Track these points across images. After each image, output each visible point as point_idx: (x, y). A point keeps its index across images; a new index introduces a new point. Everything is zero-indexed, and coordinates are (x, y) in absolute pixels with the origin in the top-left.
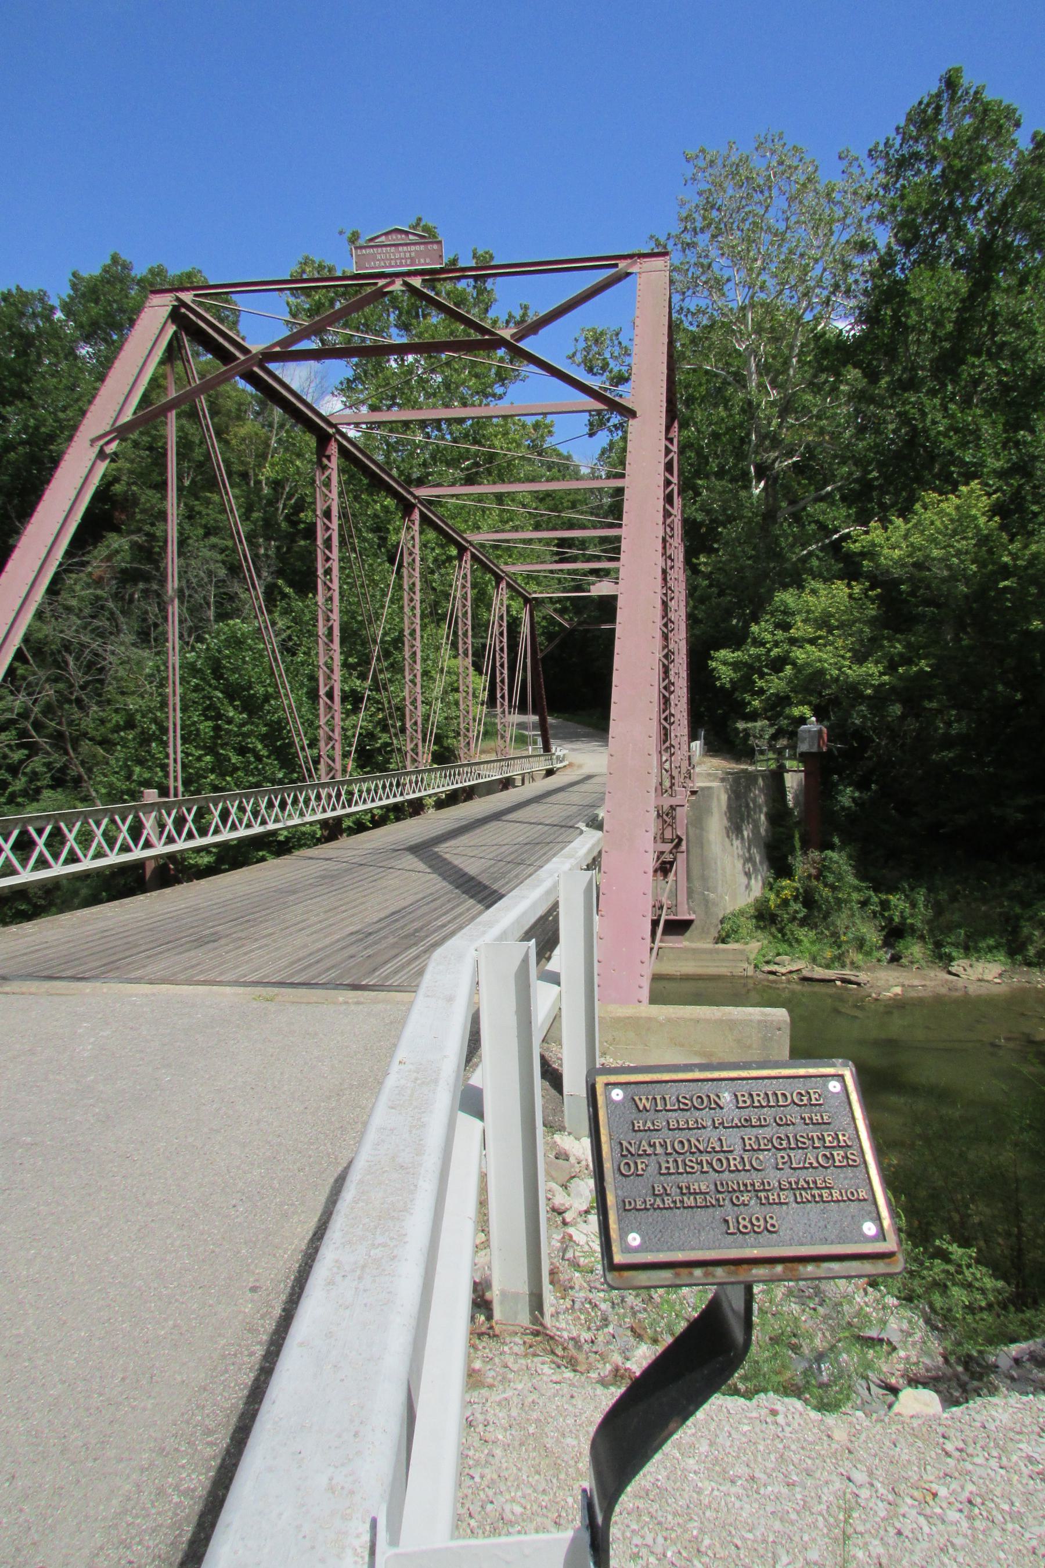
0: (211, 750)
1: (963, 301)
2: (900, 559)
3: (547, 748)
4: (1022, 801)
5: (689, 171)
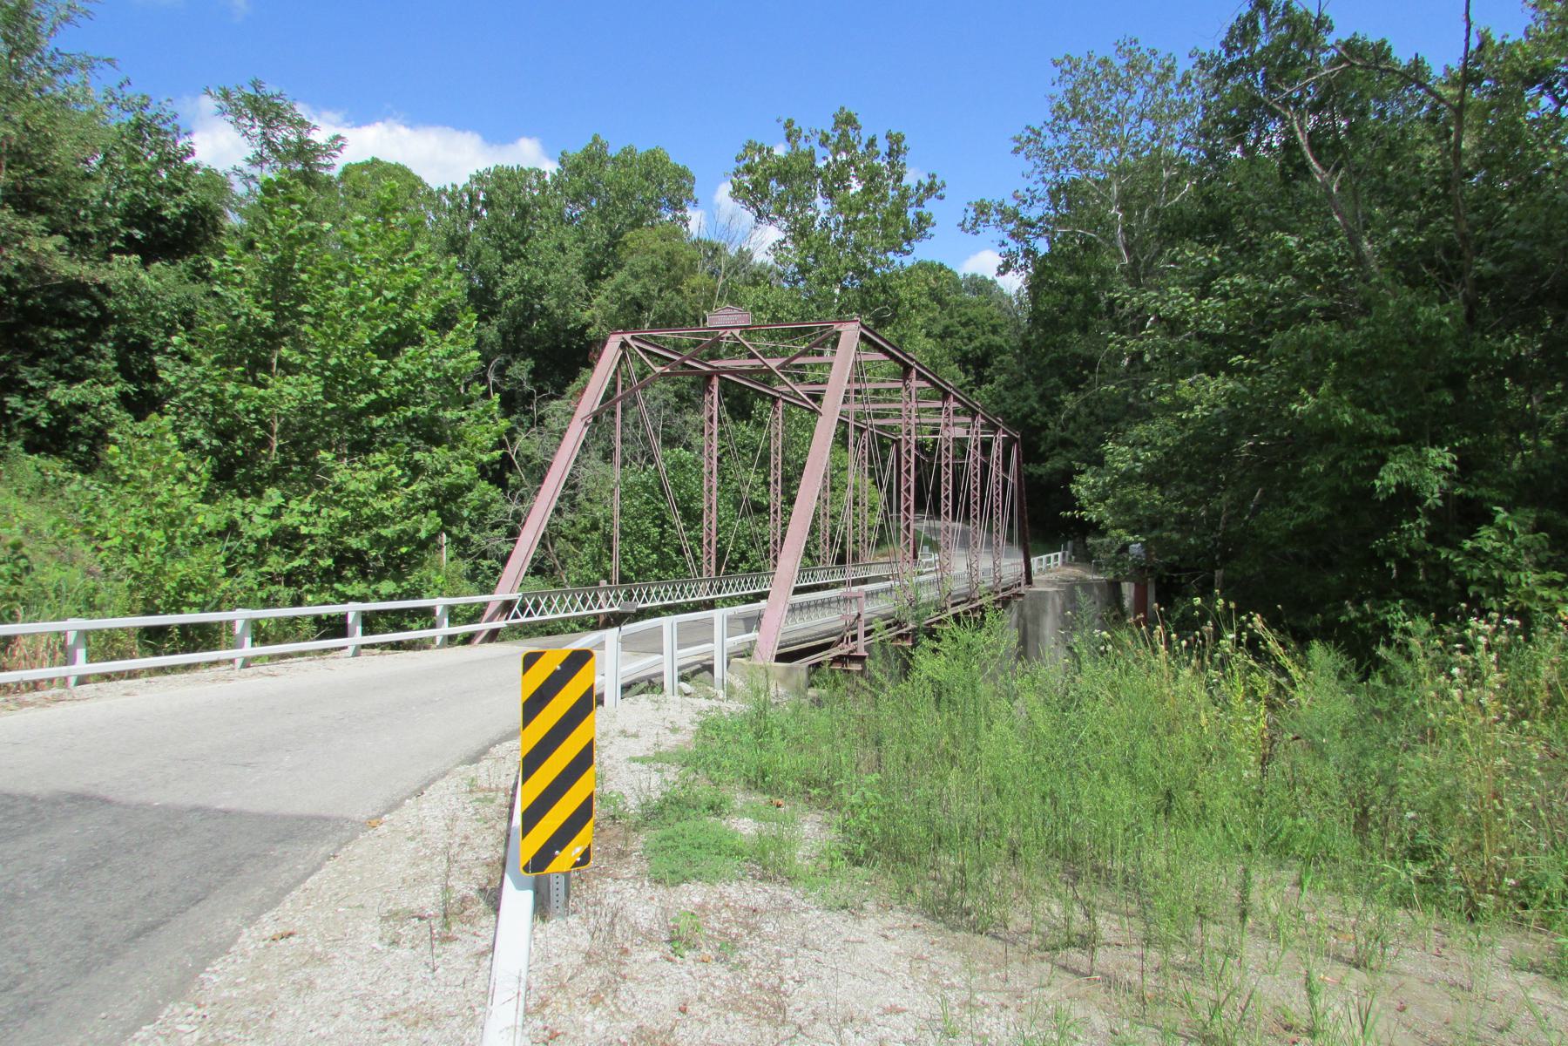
0: (656, 549)
5: (1057, 72)
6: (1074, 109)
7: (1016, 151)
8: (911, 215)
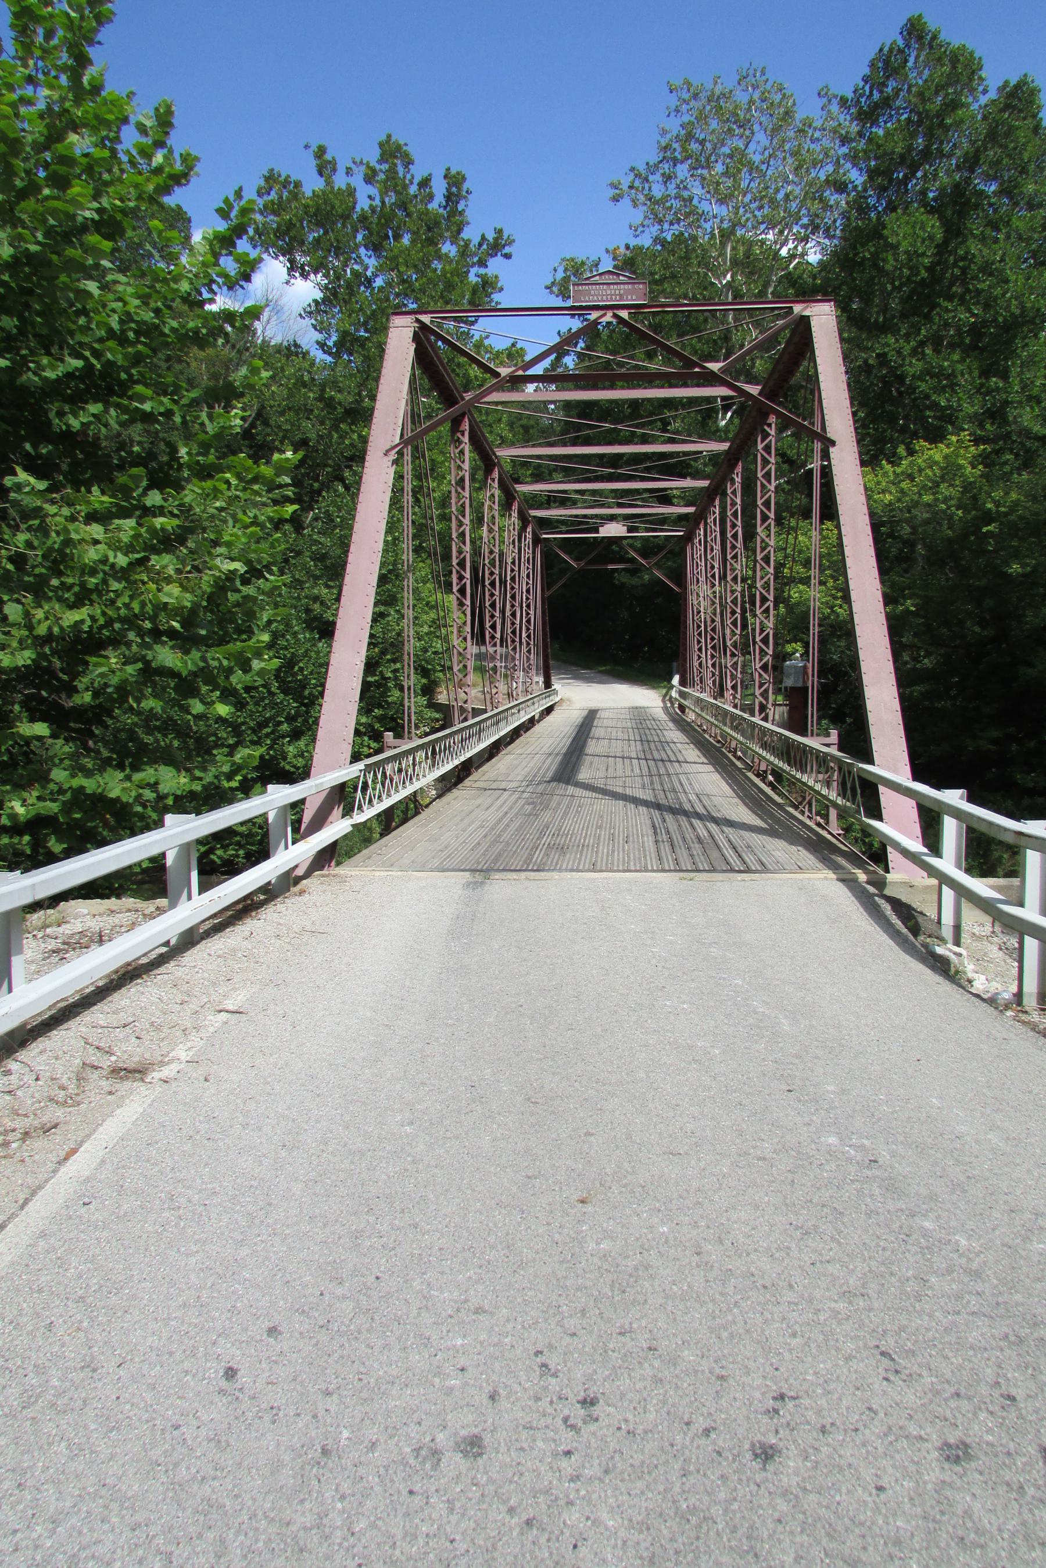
1: (937, 246)
2: (890, 504)
3: (548, 684)
4: (995, 733)
6: (684, 150)
7: (616, 199)
8: (473, 279)
